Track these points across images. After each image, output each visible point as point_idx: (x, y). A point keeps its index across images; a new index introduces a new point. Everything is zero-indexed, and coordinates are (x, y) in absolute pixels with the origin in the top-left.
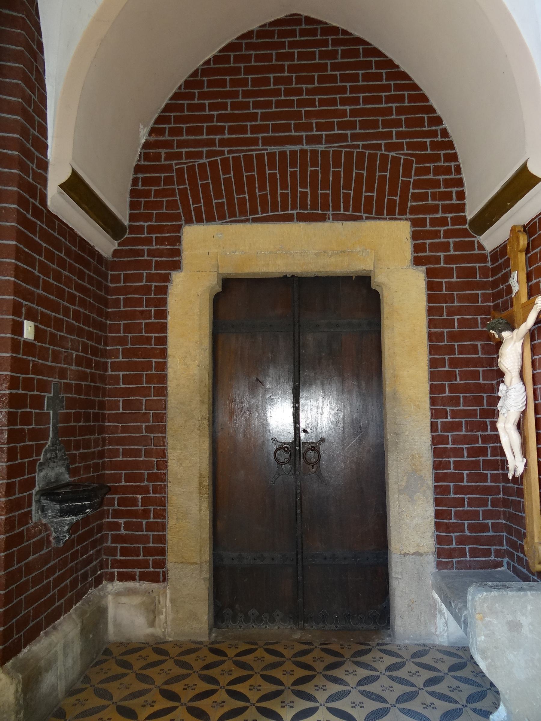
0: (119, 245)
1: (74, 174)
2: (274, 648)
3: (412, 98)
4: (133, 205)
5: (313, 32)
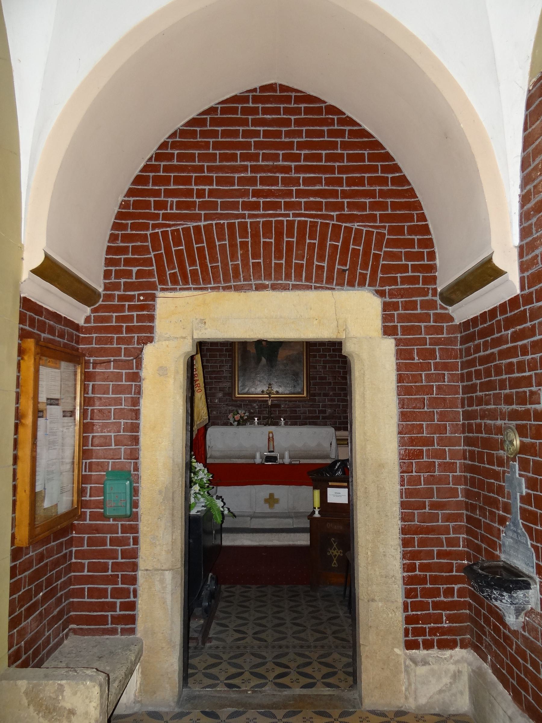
0: (93, 311)
1: (47, 257)
2: (304, 671)
3: (395, 181)
4: (107, 274)
5: (319, 111)
